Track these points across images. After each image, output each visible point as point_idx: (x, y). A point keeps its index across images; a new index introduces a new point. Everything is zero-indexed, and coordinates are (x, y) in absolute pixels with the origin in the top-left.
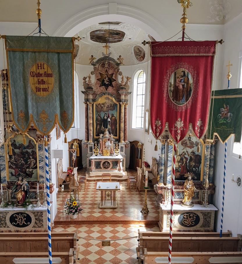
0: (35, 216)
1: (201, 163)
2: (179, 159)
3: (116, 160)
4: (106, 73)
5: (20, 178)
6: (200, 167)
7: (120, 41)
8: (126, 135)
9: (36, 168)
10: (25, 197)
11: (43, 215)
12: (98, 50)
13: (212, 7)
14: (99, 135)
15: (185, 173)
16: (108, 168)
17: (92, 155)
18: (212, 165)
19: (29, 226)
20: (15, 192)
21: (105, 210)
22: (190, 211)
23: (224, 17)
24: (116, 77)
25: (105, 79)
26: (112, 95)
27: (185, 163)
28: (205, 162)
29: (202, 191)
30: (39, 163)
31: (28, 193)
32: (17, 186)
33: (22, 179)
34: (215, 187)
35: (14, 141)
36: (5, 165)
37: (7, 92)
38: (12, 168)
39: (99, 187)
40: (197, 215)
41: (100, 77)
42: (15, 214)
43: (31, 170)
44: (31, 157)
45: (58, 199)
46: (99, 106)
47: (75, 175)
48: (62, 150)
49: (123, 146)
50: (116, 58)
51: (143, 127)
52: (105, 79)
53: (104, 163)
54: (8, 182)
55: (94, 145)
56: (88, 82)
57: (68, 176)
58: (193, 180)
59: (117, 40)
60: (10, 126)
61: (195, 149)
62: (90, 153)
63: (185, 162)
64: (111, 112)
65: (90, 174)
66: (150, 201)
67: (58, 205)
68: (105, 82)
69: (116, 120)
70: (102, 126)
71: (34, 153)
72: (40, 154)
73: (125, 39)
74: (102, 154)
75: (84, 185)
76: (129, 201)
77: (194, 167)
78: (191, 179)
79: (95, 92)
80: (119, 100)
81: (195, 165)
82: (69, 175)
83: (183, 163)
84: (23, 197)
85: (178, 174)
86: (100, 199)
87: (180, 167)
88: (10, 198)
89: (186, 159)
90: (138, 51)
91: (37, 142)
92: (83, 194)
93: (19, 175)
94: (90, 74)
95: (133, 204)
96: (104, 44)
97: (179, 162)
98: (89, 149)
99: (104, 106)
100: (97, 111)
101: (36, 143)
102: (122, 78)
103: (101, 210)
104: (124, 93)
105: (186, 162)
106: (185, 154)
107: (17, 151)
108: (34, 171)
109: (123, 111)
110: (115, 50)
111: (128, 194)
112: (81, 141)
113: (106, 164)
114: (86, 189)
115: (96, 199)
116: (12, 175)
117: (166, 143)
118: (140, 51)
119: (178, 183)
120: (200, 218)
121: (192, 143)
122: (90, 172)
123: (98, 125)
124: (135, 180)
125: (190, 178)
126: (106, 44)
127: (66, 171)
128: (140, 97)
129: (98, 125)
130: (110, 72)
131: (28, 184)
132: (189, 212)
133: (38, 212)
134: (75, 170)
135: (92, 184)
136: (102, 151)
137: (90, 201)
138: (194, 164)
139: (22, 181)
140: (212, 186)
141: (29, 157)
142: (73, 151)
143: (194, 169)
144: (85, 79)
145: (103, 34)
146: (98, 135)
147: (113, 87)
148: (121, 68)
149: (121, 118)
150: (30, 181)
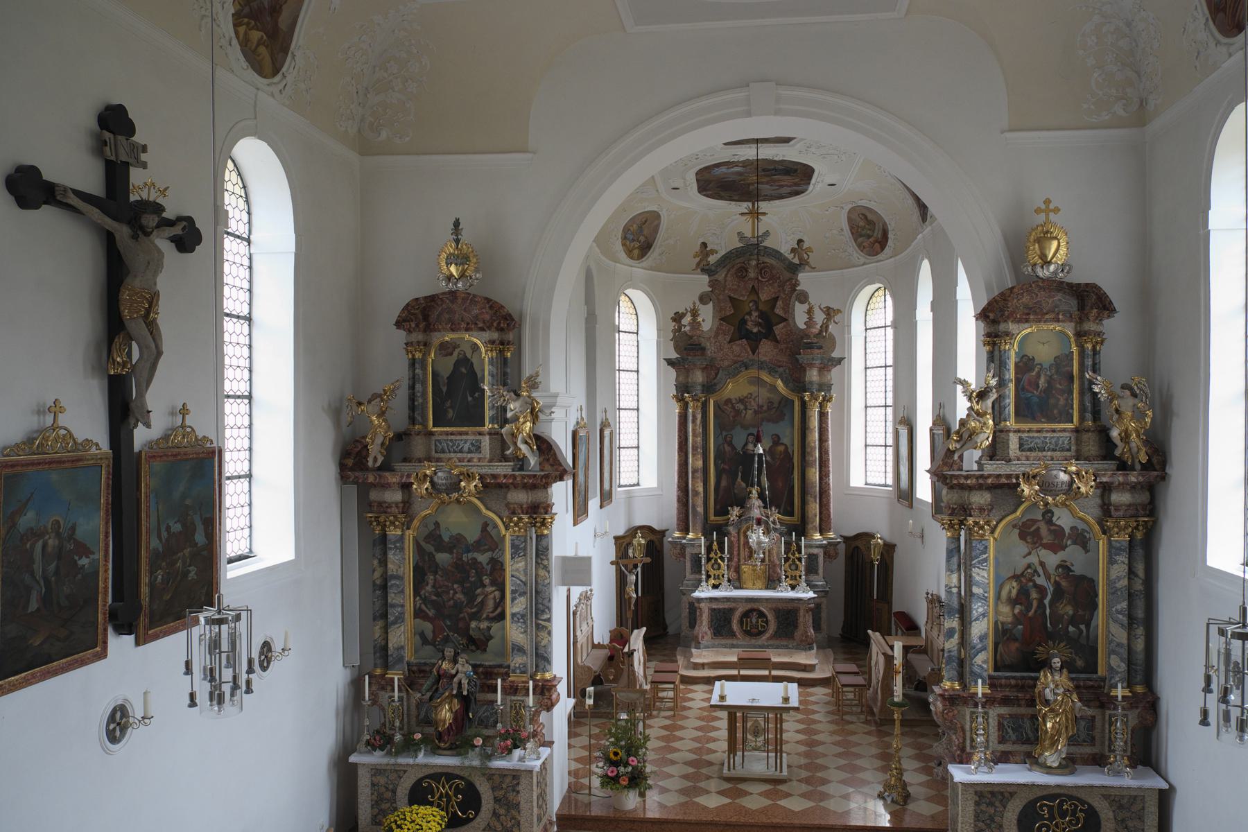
0: (493, 789)
1: (1095, 606)
2: (1014, 592)
3: (790, 606)
4: (753, 297)
5: (449, 652)
6: (1093, 624)
7: (797, 193)
8: (828, 510)
9: (502, 617)
10: (461, 720)
11: (520, 788)
12: (725, 223)
13: (1096, 75)
14: (727, 513)
15: (1040, 645)
16: (760, 633)
17: (697, 585)
18: (1140, 613)
19: (472, 824)
20: (431, 699)
21: (742, 786)
22: (1062, 791)
23: (1143, 103)
24: (788, 308)
25: (747, 317)
26: (772, 371)
27: (1038, 607)
28: (1110, 605)
29: (1108, 712)
30: (513, 599)
31: (473, 705)
32: (439, 677)
33: (456, 654)
34: (1158, 699)
35: (437, 524)
36: (403, 606)
37: (424, 368)
38: (425, 617)
39: (722, 698)
40: (1090, 805)
41: (729, 311)
42: (430, 776)
43: (484, 625)
44: (486, 580)
45: (573, 741)
46: (728, 409)
47: (635, 654)
48: (589, 559)
49: (815, 551)
50: (785, 249)
51: (890, 482)
52: (747, 317)
53: (746, 614)
54: (409, 664)
55: (709, 549)
56: (688, 328)
57: (611, 658)
58: (1070, 672)
59: (789, 190)
60: (426, 476)
61: (1073, 555)
62: (692, 577)
63: (1035, 604)
64: (768, 429)
65: (691, 655)
66: (918, 757)
67: (576, 760)
68: (750, 325)
69: (788, 457)
70: (739, 480)
71: (497, 567)
72: (517, 570)
73: (817, 185)
74: (738, 583)
75: (671, 694)
76: (835, 756)
77: (1073, 621)
78: (1062, 667)
79: (713, 359)
80: (799, 386)
81: (1073, 616)
82: (616, 656)
83: (1029, 608)
84: (455, 719)
85: (1014, 646)
86: (725, 746)
87: (1017, 619)
88: (413, 720)
89: (1042, 591)
90: (862, 224)
91: (507, 528)
92: (665, 728)
93: (447, 640)
94: (698, 303)
95: (859, 783)
96: (745, 206)
97: (1013, 602)
98: (688, 565)
99: (746, 409)
100: (720, 426)
101: (503, 531)
102: (810, 312)
103: (727, 786)
104: (817, 362)
105: (1041, 605)
106: (1035, 571)
107: (443, 558)
108: (495, 627)
109: (814, 422)
110: (783, 222)
111: (833, 733)
112: (662, 533)
113: (754, 620)
114: (677, 707)
115: (711, 746)
116: (425, 641)
117: (963, 533)
118: (869, 222)
119: (1013, 682)
120: (1102, 816)
121: (1058, 532)
122: (694, 650)
123: (724, 476)
124: (860, 680)
125: (1056, 662)
126: (750, 204)
127: (607, 642)
128: (876, 376)
129: (724, 476)
130: (764, 296)
131: (475, 673)
132: (1059, 796)
133: (503, 773)
134: (637, 640)
135: (699, 691)
136: (738, 570)
137: (689, 751)
138: (1069, 610)
139: (455, 662)
140: (1144, 694)
141: (481, 581)
142: (631, 566)
143: (1071, 629)
144: (678, 318)
145: (740, 174)
146: (722, 511)
147: (777, 341)
148: (805, 280)
149: (808, 450)
150: (481, 666)
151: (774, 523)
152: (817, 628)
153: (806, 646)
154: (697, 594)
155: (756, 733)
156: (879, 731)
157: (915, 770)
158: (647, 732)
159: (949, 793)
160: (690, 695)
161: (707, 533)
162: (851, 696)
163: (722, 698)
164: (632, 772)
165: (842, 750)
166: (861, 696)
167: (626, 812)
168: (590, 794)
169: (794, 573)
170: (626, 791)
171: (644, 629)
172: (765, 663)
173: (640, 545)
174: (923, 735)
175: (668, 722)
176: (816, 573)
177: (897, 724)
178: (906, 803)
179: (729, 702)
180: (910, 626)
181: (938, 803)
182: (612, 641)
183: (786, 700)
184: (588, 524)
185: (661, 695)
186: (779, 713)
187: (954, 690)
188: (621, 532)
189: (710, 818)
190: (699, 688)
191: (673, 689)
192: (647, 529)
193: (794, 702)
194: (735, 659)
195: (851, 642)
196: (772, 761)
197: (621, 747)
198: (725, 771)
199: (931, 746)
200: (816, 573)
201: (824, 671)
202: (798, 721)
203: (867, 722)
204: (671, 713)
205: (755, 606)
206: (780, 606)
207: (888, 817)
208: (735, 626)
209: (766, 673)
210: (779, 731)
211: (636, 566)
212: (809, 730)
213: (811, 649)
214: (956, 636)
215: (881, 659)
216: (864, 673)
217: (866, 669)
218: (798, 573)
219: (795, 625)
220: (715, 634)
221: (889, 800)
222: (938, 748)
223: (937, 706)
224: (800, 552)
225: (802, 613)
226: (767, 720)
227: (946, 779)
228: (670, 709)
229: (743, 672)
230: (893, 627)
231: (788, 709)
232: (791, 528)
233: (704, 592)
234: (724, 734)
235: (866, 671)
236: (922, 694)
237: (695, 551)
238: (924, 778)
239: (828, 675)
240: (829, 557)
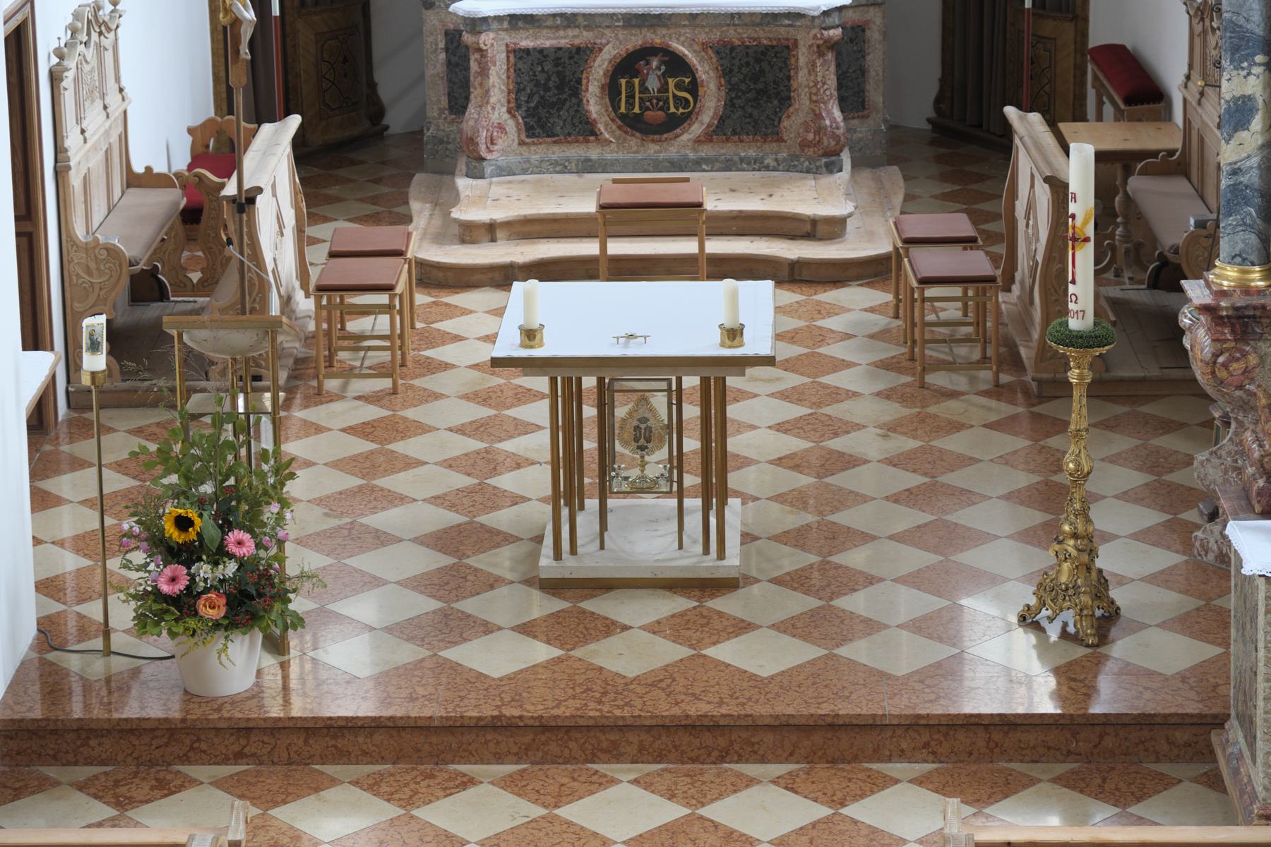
3: (765, 36)
16: (673, 124)
21: (600, 606)
39: (530, 335)
47: (263, 204)
53: (628, 66)
57: (191, 215)
65: (455, 198)
75: (383, 323)
76: (895, 499)
82: (204, 214)
113: (653, 84)
114: (403, 365)
122: (462, 183)
124: (977, 263)
127: (181, 161)
152: (852, 97)
153: (818, 158)
155: (643, 438)
156: (1036, 417)
157: (1136, 536)
159: (1232, 602)
160: (447, 326)
162: (952, 312)
164: (237, 580)
166: (981, 310)
167: (219, 703)
168: (107, 652)
170: (219, 638)
171: (295, 121)
172: (686, 217)
174: (1168, 426)
175: (372, 412)
177: (1079, 398)
178: (1103, 638)
180: (1140, 91)
181: (1203, 635)
183: (733, 334)
185: (356, 325)
186: (716, 377)
187: (1247, 291)
189: (489, 711)
191: (388, 309)
193: (758, 342)
194: (588, 206)
195: (960, 147)
196: (693, 522)
197: (201, 503)
198: (546, 560)
199: (1189, 461)
201: (871, 236)
202: (783, 395)
203: (997, 392)
204: (386, 383)
205: (655, 38)
206: (733, 35)
207: (1051, 682)
208: (594, 104)
209: (688, 246)
210: (715, 427)
212: (818, 420)
213: (833, 167)
214: (1257, 123)
215: (1043, 194)
216: (992, 238)
217: (999, 227)
219: (781, 96)
221: (1053, 633)
222: (1207, 468)
223: (1200, 340)
225: (803, 56)
227: (1226, 559)
228: (381, 371)
229: (617, 247)
230: (1091, 94)
231: (741, 364)
234: (539, 443)
235: (996, 231)
236: (1164, 298)
238: (1165, 559)
239: (882, 246)
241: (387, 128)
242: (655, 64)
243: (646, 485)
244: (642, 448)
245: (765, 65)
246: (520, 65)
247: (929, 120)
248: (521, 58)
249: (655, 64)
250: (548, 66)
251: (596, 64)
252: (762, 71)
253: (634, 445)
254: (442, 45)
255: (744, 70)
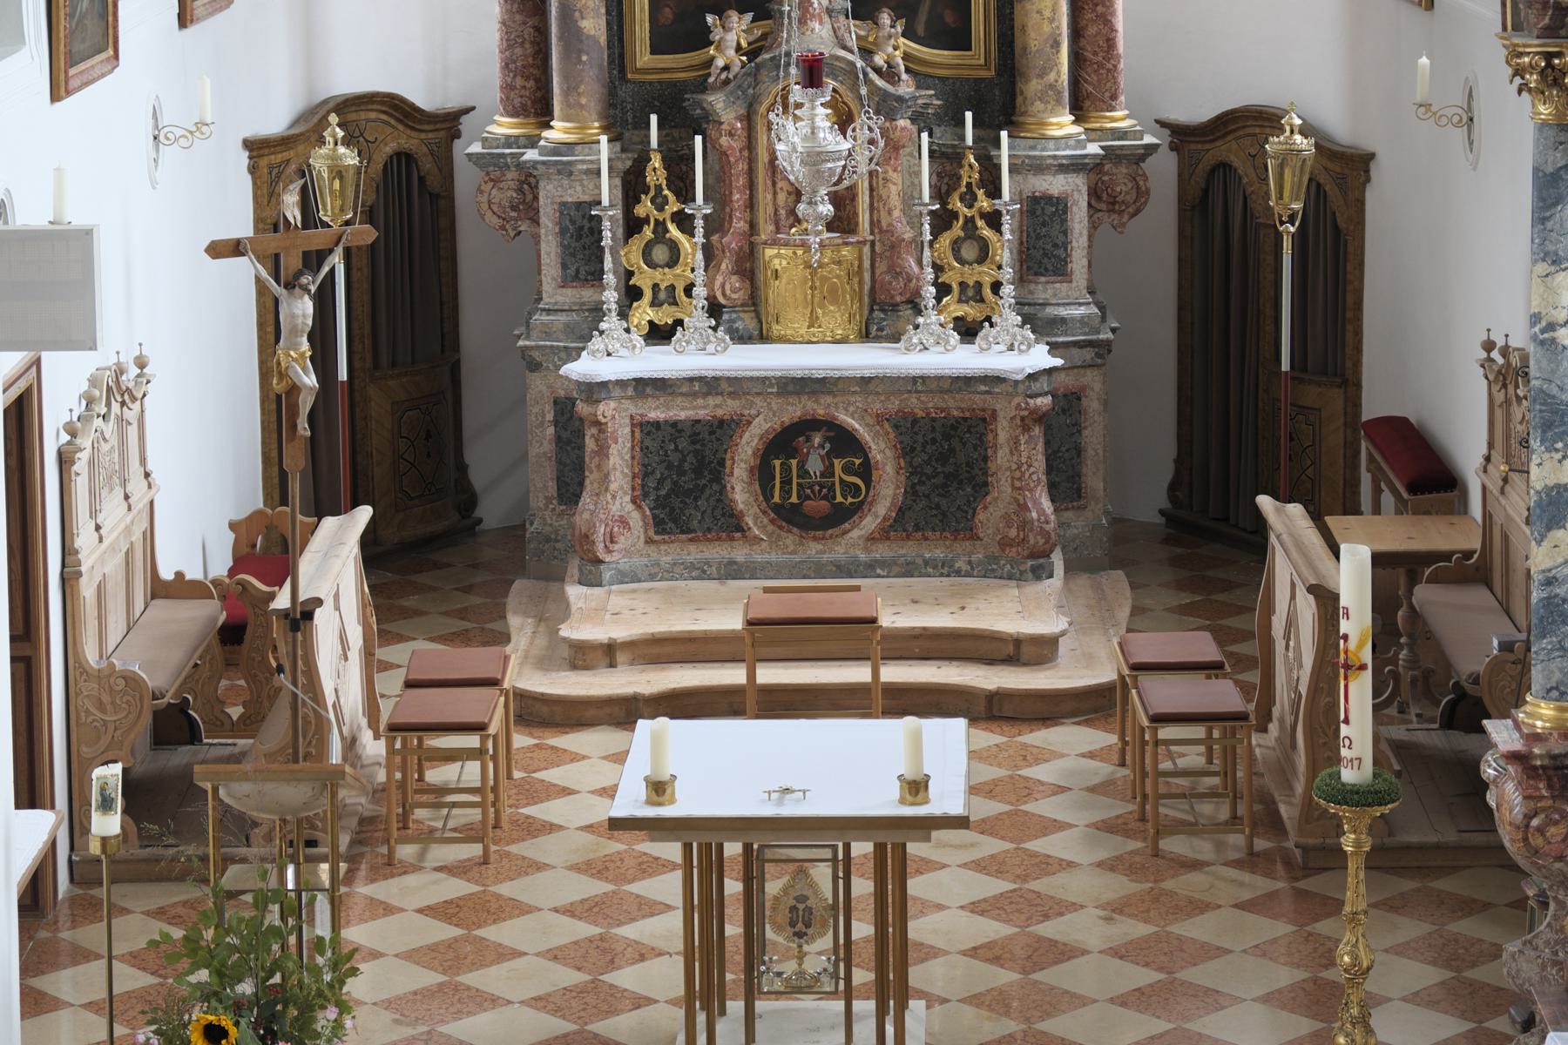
3: (955, 405)
8: (1106, 21)
14: (701, 38)
16: (839, 517)
39: (659, 789)
47: (324, 623)
49: (1056, 185)
53: (784, 443)
55: (632, 185)
57: (231, 634)
65: (565, 612)
74: (748, 316)
75: (471, 772)
76: (1122, 1001)
82: (248, 631)
92: (441, 911)
98: (550, 249)
111: (1116, 909)
112: (449, 123)
113: (815, 465)
114: (497, 826)
122: (574, 592)
124: (1223, 695)
127: (220, 566)
134: (332, 562)
136: (748, 266)
151: (890, 74)
152: (1065, 483)
153: (1023, 560)
154: (587, 367)
155: (801, 922)
156: (1301, 894)
158: (354, 934)
160: (553, 775)
161: (621, 121)
162: (1193, 758)
163: (659, 789)
165: (1146, 977)
166: (1230, 755)
169: (973, 274)
171: (364, 513)
172: (855, 635)
173: (338, 172)
174: (1469, 907)
175: (457, 888)
176: (1060, 270)
177: (1355, 872)
179: (684, 805)
180: (1428, 476)
182: (241, 562)
183: (916, 787)
184: (110, 98)
185: (437, 775)
186: (893, 843)
188: (275, 122)
190: (590, 741)
192: (367, 113)
193: (947, 798)
195: (1200, 546)
197: (238, 1007)
199: (1496, 953)
200: (1060, 270)
201: (1089, 660)
202: (979, 866)
203: (1252, 861)
204: (475, 850)
205: (818, 408)
206: (916, 404)
209: (859, 673)
210: (893, 907)
211: (314, 260)
213: (1041, 572)
215: (1307, 608)
217: (1250, 648)
218: (986, 274)
220: (660, 526)
224: (995, 193)
225: (1003, 432)
226: (844, 868)
228: (469, 834)
229: (769, 675)
230: (1366, 479)
231: (926, 826)
232: (958, 96)
233: (614, 357)
234: (668, 928)
235: (1247, 654)
236: (1463, 741)
237: (576, 193)
239: (1104, 673)
240: (1113, 205)
241: (480, 521)
242: (817, 440)
243: (804, 983)
244: (800, 935)
245: (955, 443)
246: (647, 442)
247: (1162, 512)
248: (648, 433)
249: (817, 440)
250: (683, 444)
251: (744, 441)
252: (952, 450)
253: (790, 931)
254: (550, 417)
255: (929, 449)
